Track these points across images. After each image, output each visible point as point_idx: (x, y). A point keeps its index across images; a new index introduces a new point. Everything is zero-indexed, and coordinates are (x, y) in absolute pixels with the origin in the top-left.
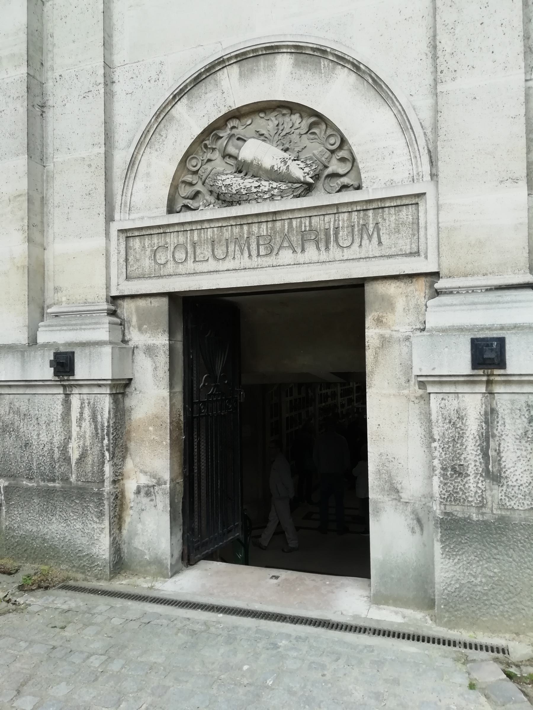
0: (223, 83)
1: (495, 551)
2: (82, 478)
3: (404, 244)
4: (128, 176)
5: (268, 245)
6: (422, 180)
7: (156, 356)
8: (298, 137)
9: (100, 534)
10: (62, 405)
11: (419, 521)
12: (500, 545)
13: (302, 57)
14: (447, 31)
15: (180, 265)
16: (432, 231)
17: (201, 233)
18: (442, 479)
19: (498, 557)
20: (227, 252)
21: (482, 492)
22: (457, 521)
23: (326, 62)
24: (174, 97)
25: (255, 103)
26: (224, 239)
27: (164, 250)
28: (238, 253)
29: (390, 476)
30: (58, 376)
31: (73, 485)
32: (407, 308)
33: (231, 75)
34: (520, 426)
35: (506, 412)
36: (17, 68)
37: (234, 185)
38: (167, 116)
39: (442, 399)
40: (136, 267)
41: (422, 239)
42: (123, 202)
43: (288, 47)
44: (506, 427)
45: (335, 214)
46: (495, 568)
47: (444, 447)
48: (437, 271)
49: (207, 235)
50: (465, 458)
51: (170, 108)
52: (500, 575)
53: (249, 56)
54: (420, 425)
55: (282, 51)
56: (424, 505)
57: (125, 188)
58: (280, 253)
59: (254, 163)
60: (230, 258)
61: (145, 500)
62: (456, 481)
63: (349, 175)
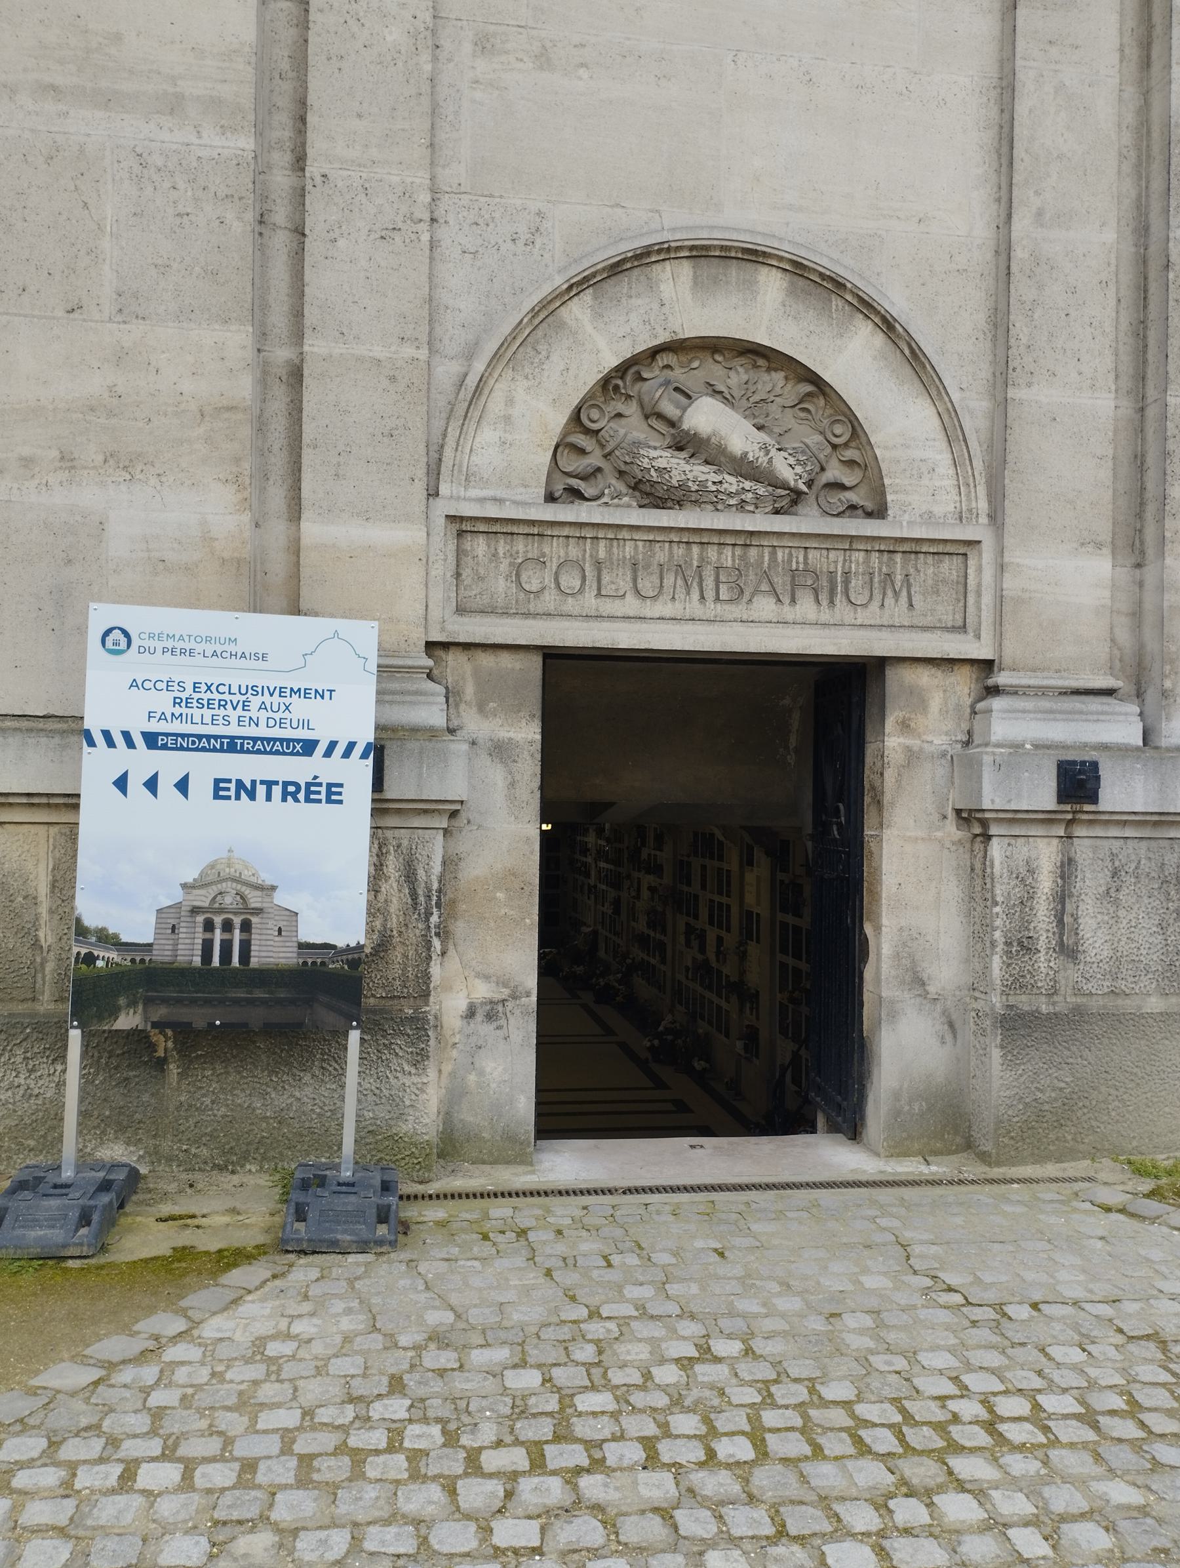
0: (662, 287)
1: (1067, 1053)
7: (514, 761)
11: (951, 1025)
13: (801, 282)
15: (570, 600)
16: (987, 599)
17: (612, 546)
19: (1071, 1060)
22: (1021, 1016)
23: (840, 303)
24: (570, 287)
26: (656, 562)
28: (681, 593)
34: (1102, 882)
35: (1086, 863)
36: (229, 134)
37: (674, 472)
38: (551, 319)
39: (1009, 844)
43: (781, 259)
45: (845, 550)
48: (990, 657)
49: (624, 552)
53: (713, 254)
55: (769, 262)
59: (713, 440)
60: (666, 597)
63: (856, 489)
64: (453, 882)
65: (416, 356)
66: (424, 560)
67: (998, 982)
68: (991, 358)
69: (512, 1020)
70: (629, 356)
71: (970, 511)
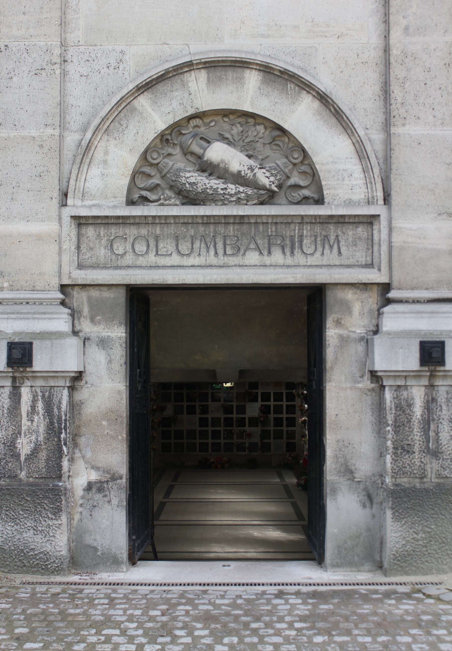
0: (190, 84)
2: (35, 474)
3: (360, 256)
4: (83, 161)
5: (234, 245)
6: (377, 204)
7: (111, 348)
8: (262, 145)
9: (56, 531)
10: (10, 398)
12: (436, 507)
14: (398, 84)
15: (141, 258)
16: (384, 248)
18: (393, 457)
20: (192, 248)
21: (424, 466)
25: (223, 109)
27: (123, 241)
28: (203, 251)
29: (346, 460)
30: (12, 367)
31: (22, 483)
32: (362, 312)
33: (199, 78)
38: (128, 106)
40: (89, 255)
41: (376, 254)
42: (77, 187)
44: (442, 413)
46: (432, 525)
47: (396, 430)
50: (412, 439)
51: (132, 98)
52: (435, 530)
54: (371, 413)
55: (250, 66)
56: (374, 482)
57: (80, 173)
58: (247, 253)
61: (98, 496)
62: (404, 457)
64: (78, 416)
65: (53, 134)
66: (58, 241)
67: (390, 471)
68: (384, 110)
69: (112, 493)
70: (172, 123)
71: (373, 197)
